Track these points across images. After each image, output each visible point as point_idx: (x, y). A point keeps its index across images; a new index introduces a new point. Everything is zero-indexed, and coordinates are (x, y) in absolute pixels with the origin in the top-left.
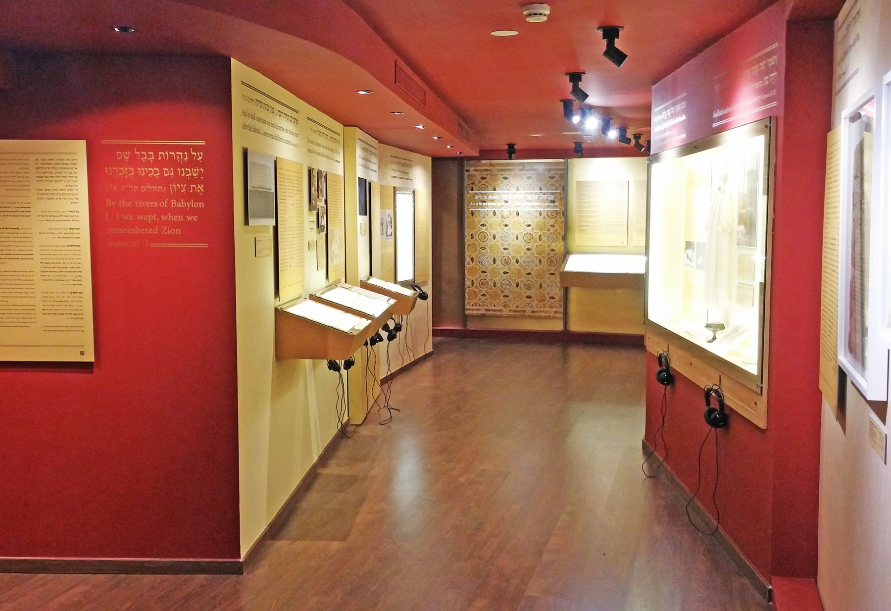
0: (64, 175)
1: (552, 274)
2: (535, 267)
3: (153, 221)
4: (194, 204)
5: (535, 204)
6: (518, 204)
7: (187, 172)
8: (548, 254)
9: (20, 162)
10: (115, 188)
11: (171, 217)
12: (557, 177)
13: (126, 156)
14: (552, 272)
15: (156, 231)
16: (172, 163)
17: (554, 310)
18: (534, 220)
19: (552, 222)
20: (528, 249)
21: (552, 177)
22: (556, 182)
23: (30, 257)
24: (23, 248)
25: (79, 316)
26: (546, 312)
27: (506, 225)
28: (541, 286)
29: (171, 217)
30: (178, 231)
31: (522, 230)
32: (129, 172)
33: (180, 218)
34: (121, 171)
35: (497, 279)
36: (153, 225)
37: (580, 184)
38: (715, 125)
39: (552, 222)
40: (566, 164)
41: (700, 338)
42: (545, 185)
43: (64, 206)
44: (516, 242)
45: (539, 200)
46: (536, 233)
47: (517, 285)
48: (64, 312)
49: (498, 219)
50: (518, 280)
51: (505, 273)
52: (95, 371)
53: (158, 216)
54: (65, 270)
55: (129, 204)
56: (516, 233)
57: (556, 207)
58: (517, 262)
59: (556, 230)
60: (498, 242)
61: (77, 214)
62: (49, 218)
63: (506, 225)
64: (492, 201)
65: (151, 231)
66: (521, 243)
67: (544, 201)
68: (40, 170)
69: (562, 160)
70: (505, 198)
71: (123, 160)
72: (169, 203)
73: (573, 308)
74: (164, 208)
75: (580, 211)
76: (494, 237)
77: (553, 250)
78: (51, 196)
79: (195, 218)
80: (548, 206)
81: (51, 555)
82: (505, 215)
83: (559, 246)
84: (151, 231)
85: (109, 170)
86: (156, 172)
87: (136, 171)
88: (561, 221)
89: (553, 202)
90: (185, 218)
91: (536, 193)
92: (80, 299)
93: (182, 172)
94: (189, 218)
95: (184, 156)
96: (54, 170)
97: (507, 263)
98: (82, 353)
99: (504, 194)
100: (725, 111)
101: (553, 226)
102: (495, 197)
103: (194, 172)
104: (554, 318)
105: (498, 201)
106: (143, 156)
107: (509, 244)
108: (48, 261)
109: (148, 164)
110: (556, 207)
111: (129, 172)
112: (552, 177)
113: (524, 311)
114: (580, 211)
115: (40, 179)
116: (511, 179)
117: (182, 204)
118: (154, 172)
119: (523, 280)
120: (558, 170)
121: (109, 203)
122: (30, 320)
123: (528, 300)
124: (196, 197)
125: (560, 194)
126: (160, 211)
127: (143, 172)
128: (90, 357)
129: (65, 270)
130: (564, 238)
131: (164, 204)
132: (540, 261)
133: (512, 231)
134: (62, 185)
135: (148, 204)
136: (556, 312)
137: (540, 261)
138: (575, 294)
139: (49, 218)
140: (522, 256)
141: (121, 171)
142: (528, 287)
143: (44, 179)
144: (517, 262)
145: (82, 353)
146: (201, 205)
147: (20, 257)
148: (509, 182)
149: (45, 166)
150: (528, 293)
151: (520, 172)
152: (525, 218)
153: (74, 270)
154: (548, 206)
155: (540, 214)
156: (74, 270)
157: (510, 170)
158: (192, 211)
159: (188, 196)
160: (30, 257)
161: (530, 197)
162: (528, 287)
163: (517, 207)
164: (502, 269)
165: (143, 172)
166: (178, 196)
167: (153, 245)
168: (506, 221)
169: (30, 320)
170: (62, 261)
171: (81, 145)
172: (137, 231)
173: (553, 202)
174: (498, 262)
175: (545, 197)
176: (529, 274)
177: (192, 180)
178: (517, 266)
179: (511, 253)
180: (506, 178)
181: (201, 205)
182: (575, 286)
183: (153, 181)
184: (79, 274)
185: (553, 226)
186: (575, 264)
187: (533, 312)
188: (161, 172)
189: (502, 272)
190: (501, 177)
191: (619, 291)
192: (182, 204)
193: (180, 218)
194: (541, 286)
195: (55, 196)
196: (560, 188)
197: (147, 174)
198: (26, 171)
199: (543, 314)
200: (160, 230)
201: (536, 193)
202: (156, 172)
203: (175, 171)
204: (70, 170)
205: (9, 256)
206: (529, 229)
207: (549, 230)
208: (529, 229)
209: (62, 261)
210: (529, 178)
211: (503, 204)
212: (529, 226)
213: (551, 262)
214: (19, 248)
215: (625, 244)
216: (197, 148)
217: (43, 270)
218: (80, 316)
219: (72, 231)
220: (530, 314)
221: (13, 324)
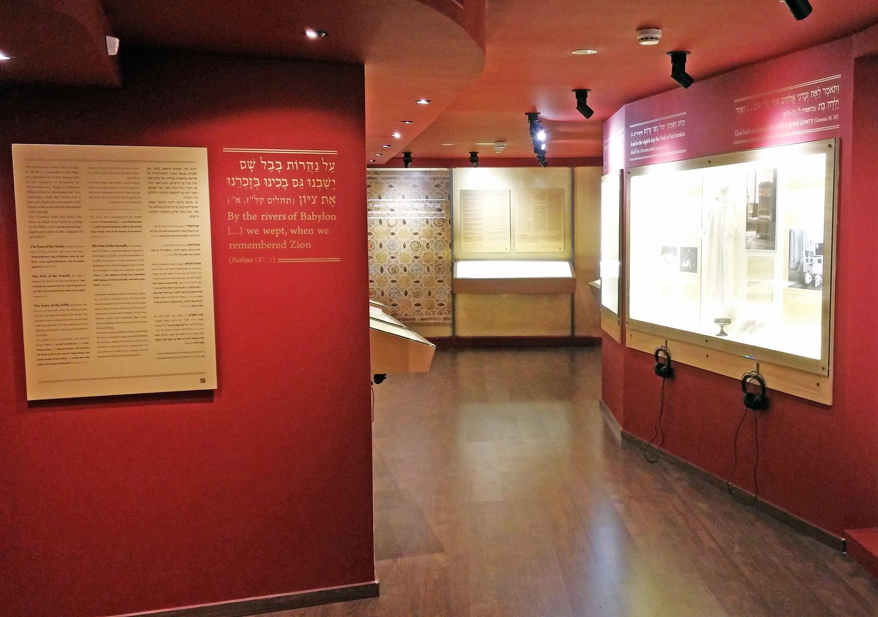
0: (181, 185)
1: (440, 281)
2: (423, 276)
3: (280, 235)
4: (324, 217)
5: (422, 212)
6: (404, 212)
7: (318, 183)
8: (436, 262)
9: (128, 171)
10: (238, 200)
11: (300, 231)
12: (443, 185)
13: (251, 165)
14: (441, 279)
15: (284, 245)
16: (302, 173)
17: (444, 316)
18: (421, 228)
19: (439, 230)
20: (416, 257)
21: (438, 186)
22: (442, 190)
23: (140, 277)
24: (132, 267)
25: (198, 340)
26: (435, 319)
27: (393, 234)
28: (429, 294)
29: (300, 231)
30: (308, 245)
31: (409, 239)
32: (254, 182)
33: (311, 231)
34: (245, 182)
35: (385, 289)
36: (281, 238)
37: (464, 193)
38: (736, 143)
39: (439, 230)
40: (451, 173)
41: (712, 331)
42: (431, 193)
43: (181, 220)
44: (404, 250)
45: (425, 208)
46: (424, 241)
47: (406, 294)
48: (181, 337)
49: (384, 227)
50: (407, 289)
51: (393, 281)
52: (216, 398)
53: (287, 230)
54: (182, 290)
55: (254, 217)
56: (404, 241)
57: (442, 215)
58: (405, 270)
59: (443, 238)
60: (385, 251)
61: (197, 229)
62: (163, 234)
63: (393, 234)
64: (378, 209)
65: (278, 246)
66: (408, 251)
67: (431, 209)
68: (152, 180)
69: (446, 169)
70: (391, 206)
71: (247, 169)
72: (299, 216)
73: (461, 315)
74: (293, 221)
75: (465, 219)
76: (381, 246)
77: (440, 258)
78: (167, 209)
79: (326, 231)
80: (435, 215)
81: (196, 603)
82: (392, 223)
83: (445, 253)
84: (278, 246)
85: (232, 181)
86: (284, 183)
87: (262, 182)
88: (447, 228)
89: (440, 210)
90: (315, 231)
91: (423, 202)
92: (201, 322)
93: (312, 182)
94: (320, 231)
95: (315, 166)
96: (169, 181)
97: (395, 272)
98: (203, 381)
99: (390, 202)
100: (754, 131)
101: (440, 234)
102: (380, 206)
103: (326, 183)
104: (443, 324)
105: (384, 209)
106: (270, 165)
107: (396, 253)
108: (161, 281)
109: (275, 174)
110: (442, 215)
111: (254, 182)
112: (438, 186)
113: (413, 319)
114: (465, 219)
115: (152, 191)
116: (396, 187)
117: (313, 217)
118: (282, 183)
119: (411, 288)
120: (444, 178)
121: (231, 216)
122: (141, 348)
123: (417, 308)
124: (328, 209)
125: (446, 202)
126: (288, 225)
127: (269, 182)
128: (212, 384)
129: (182, 290)
130: (451, 246)
131: (294, 217)
132: (428, 268)
133: (399, 240)
134: (179, 197)
135: (275, 217)
136: (445, 319)
137: (428, 268)
138: (462, 300)
139: (163, 234)
140: (410, 264)
141: (245, 182)
142: (417, 295)
143: (157, 190)
144: (405, 270)
145: (203, 381)
146: (333, 217)
147: (128, 277)
148: (395, 190)
149: (159, 176)
150: (417, 301)
151: (406, 181)
152: (412, 227)
153: (193, 290)
154: (435, 215)
155: (427, 222)
156: (193, 290)
157: (395, 178)
158: (324, 224)
159: (319, 208)
160: (140, 277)
161: (416, 205)
162: (417, 295)
163: (403, 215)
164: (390, 277)
165: (269, 182)
166: (308, 208)
167: (281, 260)
168: (393, 230)
169: (141, 348)
170: (179, 281)
171: (203, 152)
172: (262, 245)
173: (440, 210)
174: (386, 270)
175: (431, 205)
176: (418, 282)
177: (324, 191)
178: (405, 274)
179: (399, 262)
180: (391, 186)
181: (333, 217)
182: (461, 292)
183: (280, 192)
184: (200, 294)
185: (440, 234)
186: (464, 271)
187: (422, 319)
188: (290, 182)
189: (389, 281)
190: (386, 186)
191: (504, 296)
192: (313, 217)
193: (311, 231)
194: (429, 294)
195: (171, 210)
196: (443, 193)
197: (274, 185)
198: (137, 181)
199: (433, 321)
200: (289, 245)
201: (423, 202)
202: (284, 183)
203: (305, 182)
204: (188, 181)
205: (114, 277)
206: (416, 238)
207: (436, 238)
208: (416, 238)
209: (179, 281)
210: (415, 186)
211: (389, 212)
212: (416, 234)
213: (439, 270)
214: (126, 268)
215: (509, 248)
216: (328, 158)
217: (157, 291)
218: (201, 340)
219: (191, 247)
220: (419, 321)
221: (119, 353)
